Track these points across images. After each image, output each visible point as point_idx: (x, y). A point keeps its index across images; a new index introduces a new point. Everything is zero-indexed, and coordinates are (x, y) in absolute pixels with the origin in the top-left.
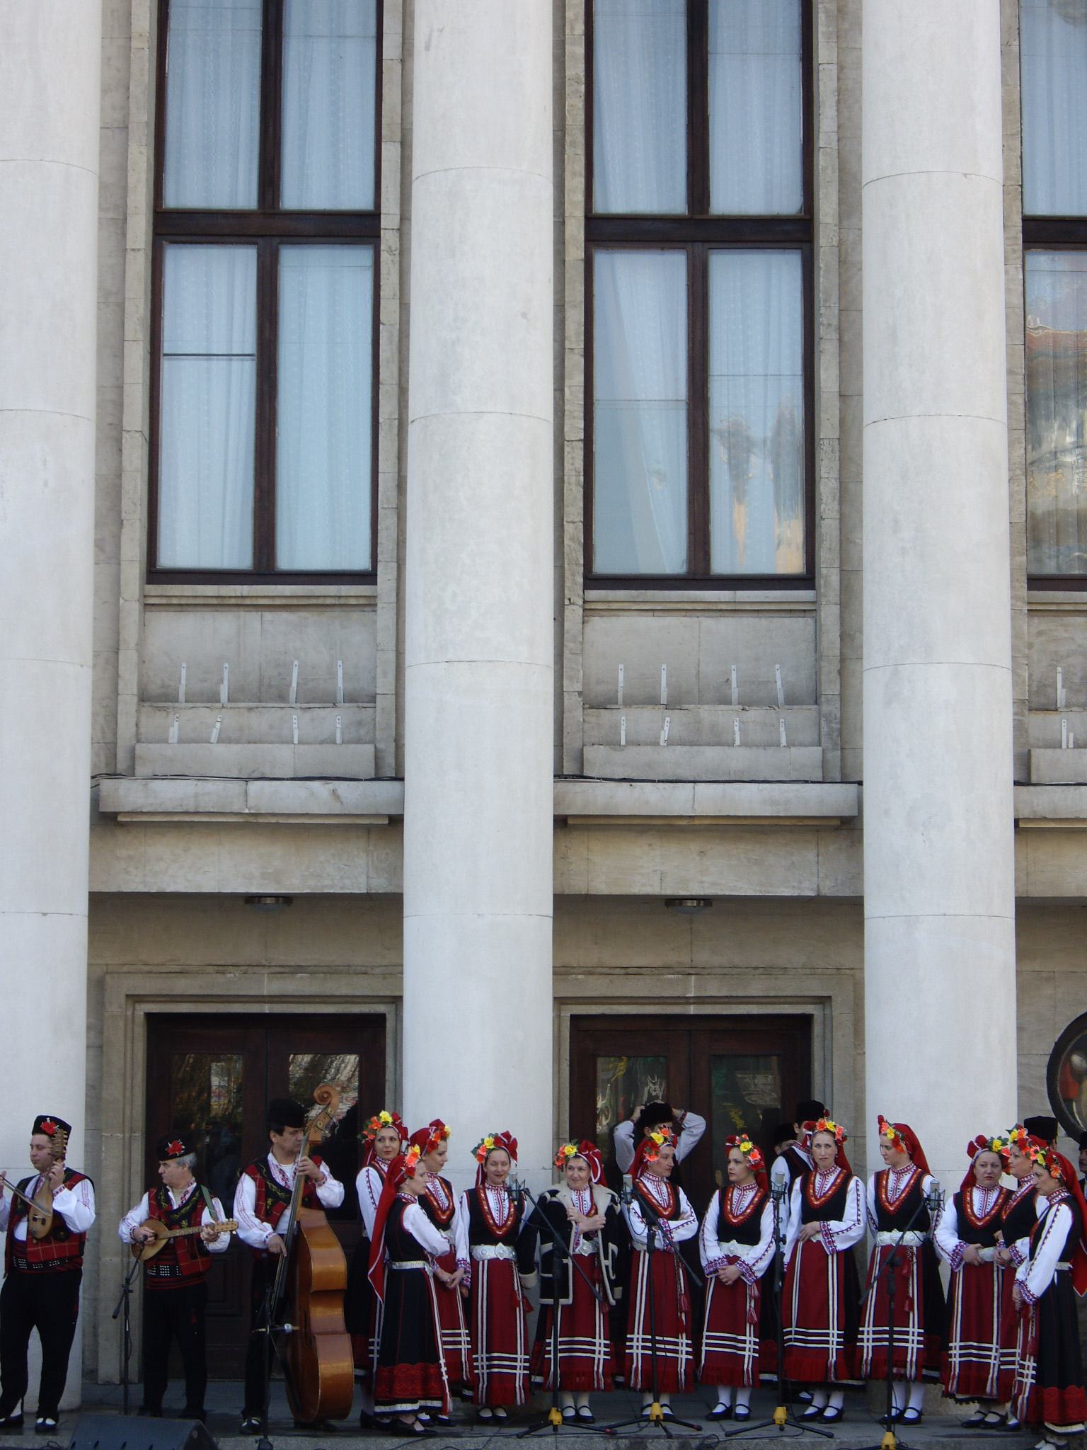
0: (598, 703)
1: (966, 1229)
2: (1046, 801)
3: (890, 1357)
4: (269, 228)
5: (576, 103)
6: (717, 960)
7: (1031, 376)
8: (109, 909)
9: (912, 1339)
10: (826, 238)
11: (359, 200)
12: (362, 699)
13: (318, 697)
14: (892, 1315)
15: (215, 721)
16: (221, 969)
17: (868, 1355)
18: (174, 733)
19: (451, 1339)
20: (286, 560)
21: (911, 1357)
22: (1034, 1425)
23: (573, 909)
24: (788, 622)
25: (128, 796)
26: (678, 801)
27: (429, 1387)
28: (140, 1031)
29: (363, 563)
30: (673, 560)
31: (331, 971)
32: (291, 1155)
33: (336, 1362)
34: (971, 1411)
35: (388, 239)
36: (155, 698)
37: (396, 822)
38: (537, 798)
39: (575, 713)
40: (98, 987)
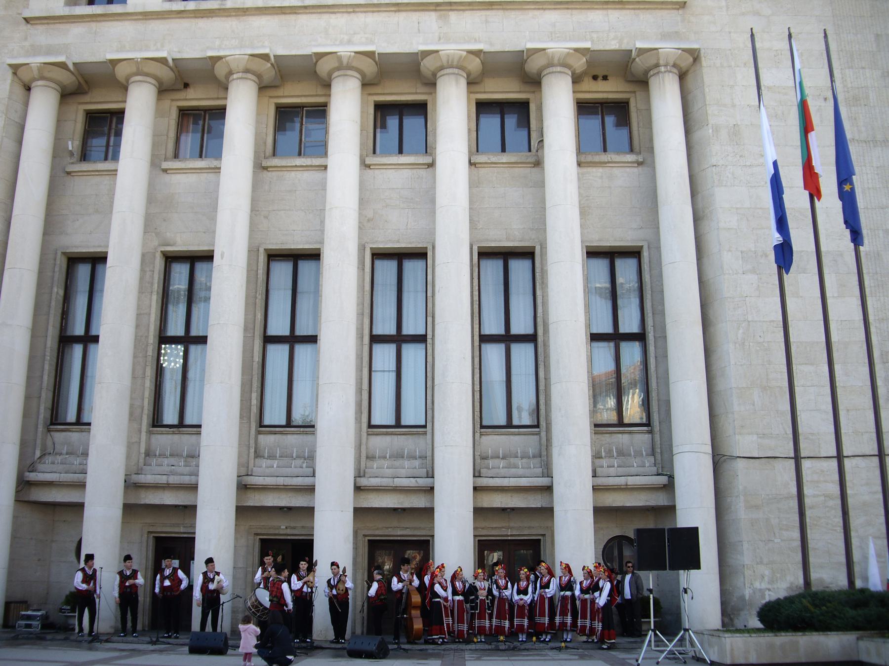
0: (484, 458)
1: (582, 591)
2: (601, 481)
3: (563, 624)
4: (399, 339)
5: (476, 306)
6: (516, 525)
7: (594, 386)
8: (358, 512)
9: (569, 620)
10: (540, 339)
11: (422, 332)
12: (423, 457)
13: (412, 457)
14: (564, 613)
15: (386, 463)
16: (387, 528)
17: (557, 624)
18: (375, 466)
19: (447, 621)
20: (403, 423)
21: (569, 624)
22: (601, 641)
23: (479, 512)
24: (532, 437)
25: (363, 482)
26: (505, 482)
27: (441, 632)
28: (366, 544)
29: (423, 423)
30: (503, 421)
31: (415, 528)
32: (406, 571)
33: (418, 625)
34: (584, 638)
35: (429, 341)
36: (370, 458)
37: (432, 488)
38: (468, 482)
39: (478, 461)
40: (356, 533)
